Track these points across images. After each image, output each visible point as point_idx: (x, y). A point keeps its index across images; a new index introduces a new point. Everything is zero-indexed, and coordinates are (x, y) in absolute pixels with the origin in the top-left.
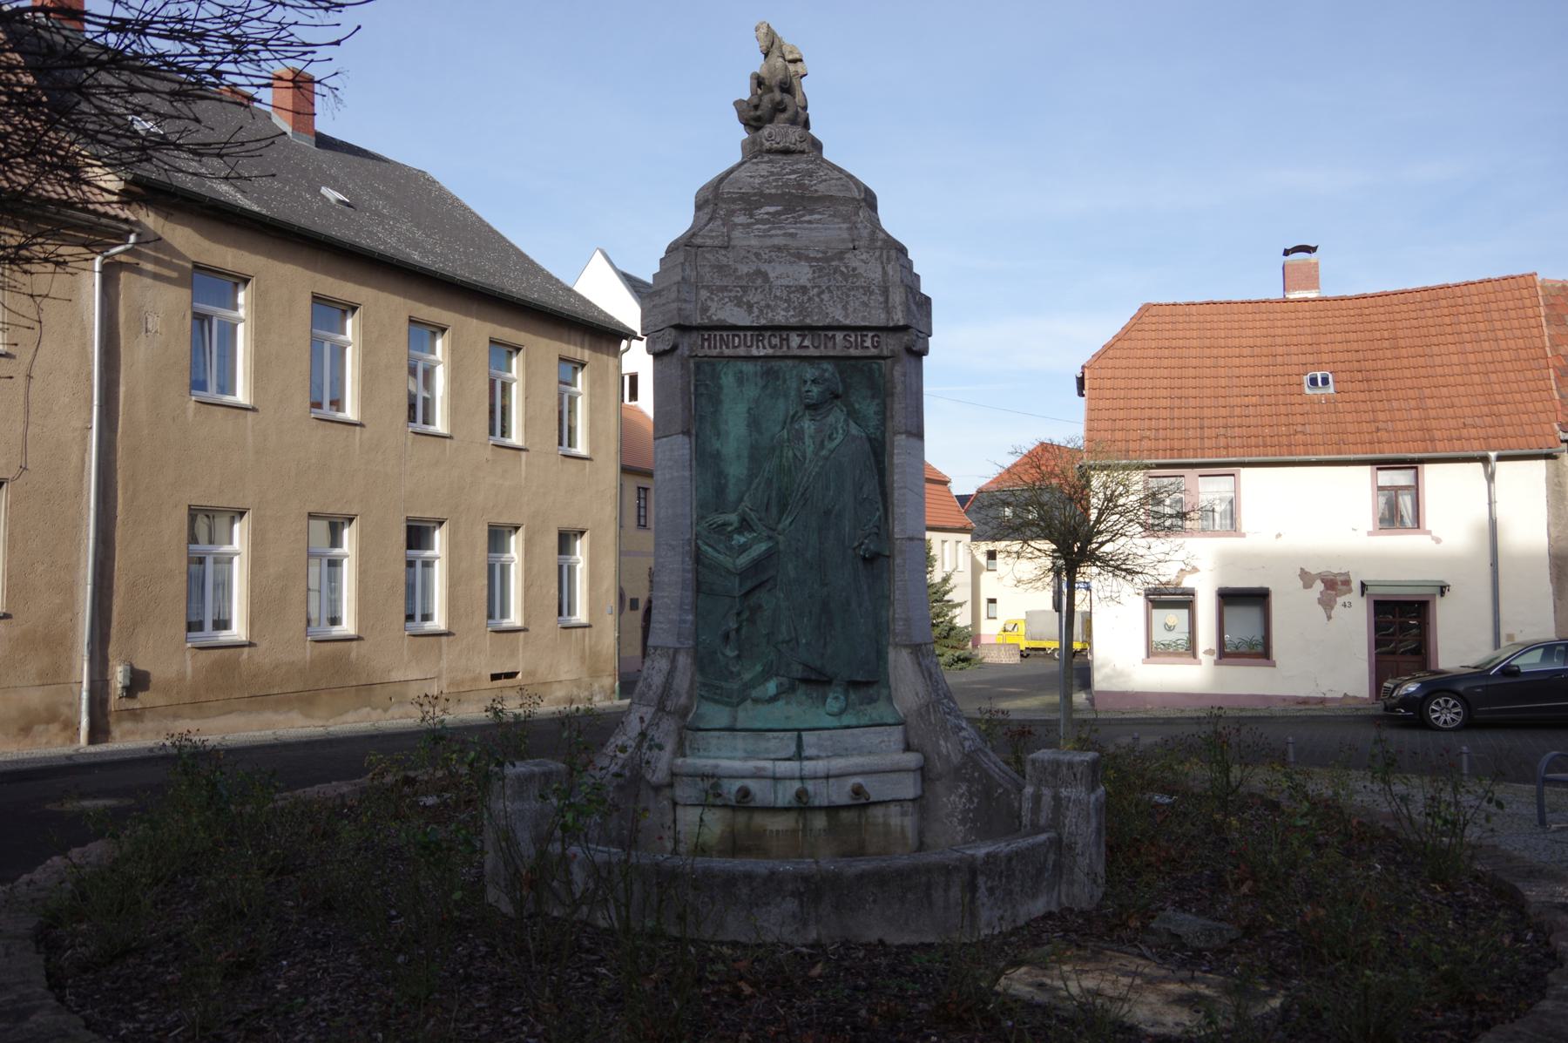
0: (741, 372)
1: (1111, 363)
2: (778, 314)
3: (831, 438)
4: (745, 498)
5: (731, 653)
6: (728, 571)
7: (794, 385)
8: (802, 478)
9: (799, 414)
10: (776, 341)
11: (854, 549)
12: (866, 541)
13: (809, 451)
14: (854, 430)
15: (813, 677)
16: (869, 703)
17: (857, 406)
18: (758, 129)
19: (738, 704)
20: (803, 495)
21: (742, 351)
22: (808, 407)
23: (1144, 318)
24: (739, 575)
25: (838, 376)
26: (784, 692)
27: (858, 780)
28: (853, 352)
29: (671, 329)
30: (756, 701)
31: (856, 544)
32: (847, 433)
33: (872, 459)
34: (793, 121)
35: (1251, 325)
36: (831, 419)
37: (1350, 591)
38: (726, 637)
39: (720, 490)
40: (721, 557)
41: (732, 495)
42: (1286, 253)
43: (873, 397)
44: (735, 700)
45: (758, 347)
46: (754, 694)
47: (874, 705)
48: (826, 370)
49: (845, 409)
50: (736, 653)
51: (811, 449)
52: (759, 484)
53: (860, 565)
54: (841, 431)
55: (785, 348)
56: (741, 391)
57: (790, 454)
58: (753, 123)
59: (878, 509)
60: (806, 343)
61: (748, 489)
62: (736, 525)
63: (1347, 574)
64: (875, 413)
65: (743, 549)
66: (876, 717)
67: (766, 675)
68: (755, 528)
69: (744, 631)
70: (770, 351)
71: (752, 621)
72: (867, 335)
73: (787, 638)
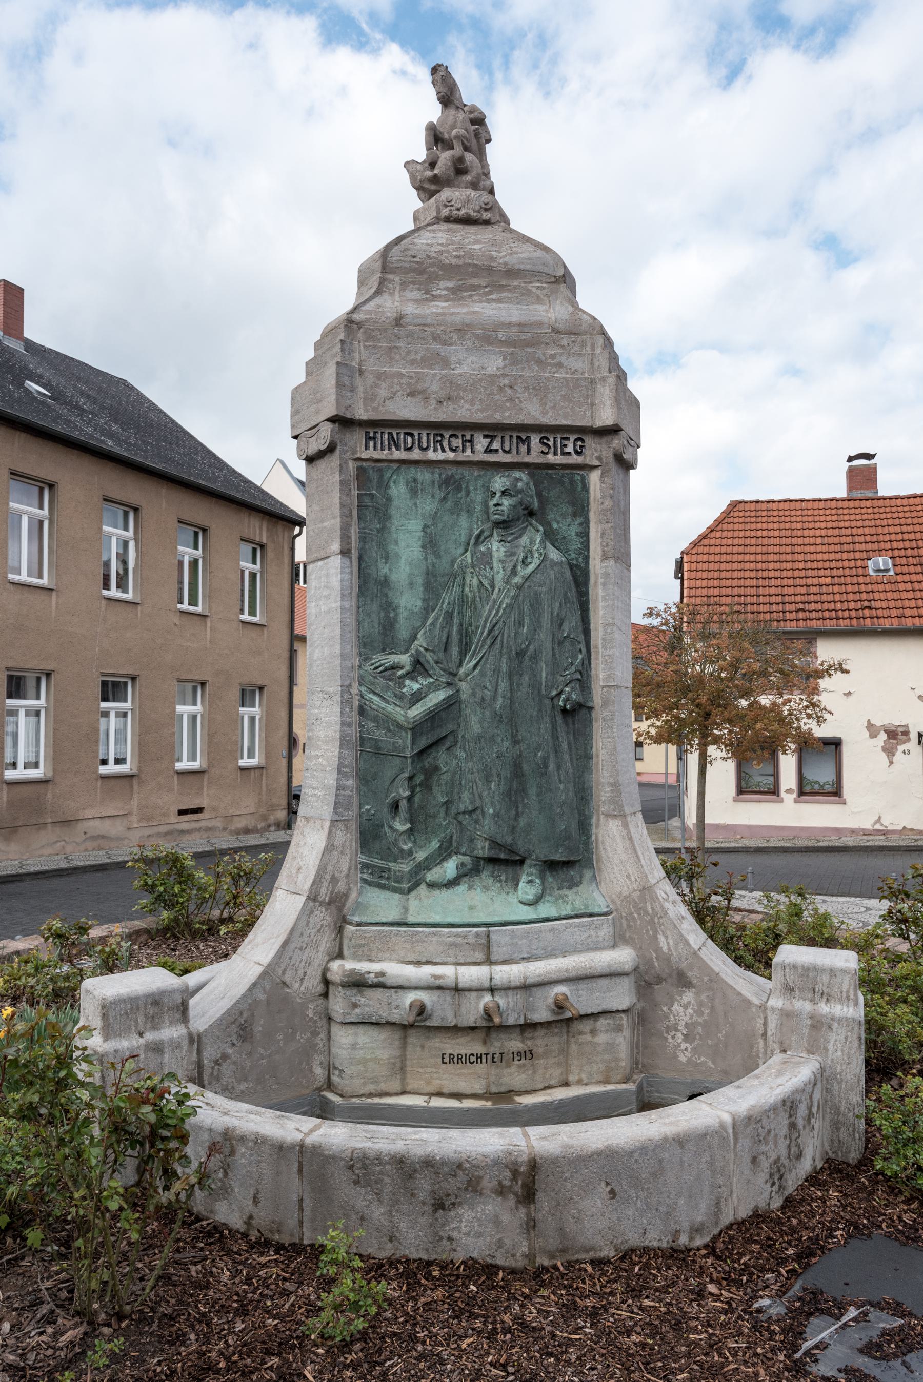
0: (415, 480)
1: (706, 550)
2: (461, 407)
3: (525, 563)
4: (419, 636)
5: (401, 826)
6: (400, 726)
7: (479, 499)
8: (490, 611)
9: (486, 534)
10: (456, 443)
11: (552, 699)
12: (567, 689)
13: (499, 578)
14: (554, 555)
15: (502, 856)
16: (570, 888)
17: (555, 526)
18: (432, 194)
19: (410, 890)
20: (490, 632)
21: (416, 455)
22: (498, 524)
23: (731, 514)
24: (412, 729)
25: (533, 487)
26: (466, 875)
27: (561, 989)
28: (551, 458)
29: (328, 423)
30: (432, 885)
31: (554, 693)
32: (545, 558)
33: (574, 589)
34: (474, 186)
35: (822, 518)
36: (525, 540)
37: (909, 740)
38: (395, 806)
39: (389, 626)
40: (390, 708)
41: (403, 631)
42: (850, 459)
43: (575, 515)
44: (405, 886)
45: (435, 450)
46: (430, 876)
47: (575, 890)
48: (519, 480)
49: (541, 528)
50: (408, 826)
51: (501, 575)
52: (436, 619)
53: (559, 719)
54: (536, 555)
55: (469, 452)
56: (415, 504)
57: (475, 582)
58: (427, 185)
59: (580, 650)
60: (496, 445)
61: (424, 624)
62: (408, 668)
63: (907, 726)
64: (577, 534)
65: (417, 698)
66: (580, 907)
67: (444, 853)
68: (431, 672)
69: (417, 799)
70: (451, 455)
71: (427, 786)
72: (568, 439)
73: (470, 808)
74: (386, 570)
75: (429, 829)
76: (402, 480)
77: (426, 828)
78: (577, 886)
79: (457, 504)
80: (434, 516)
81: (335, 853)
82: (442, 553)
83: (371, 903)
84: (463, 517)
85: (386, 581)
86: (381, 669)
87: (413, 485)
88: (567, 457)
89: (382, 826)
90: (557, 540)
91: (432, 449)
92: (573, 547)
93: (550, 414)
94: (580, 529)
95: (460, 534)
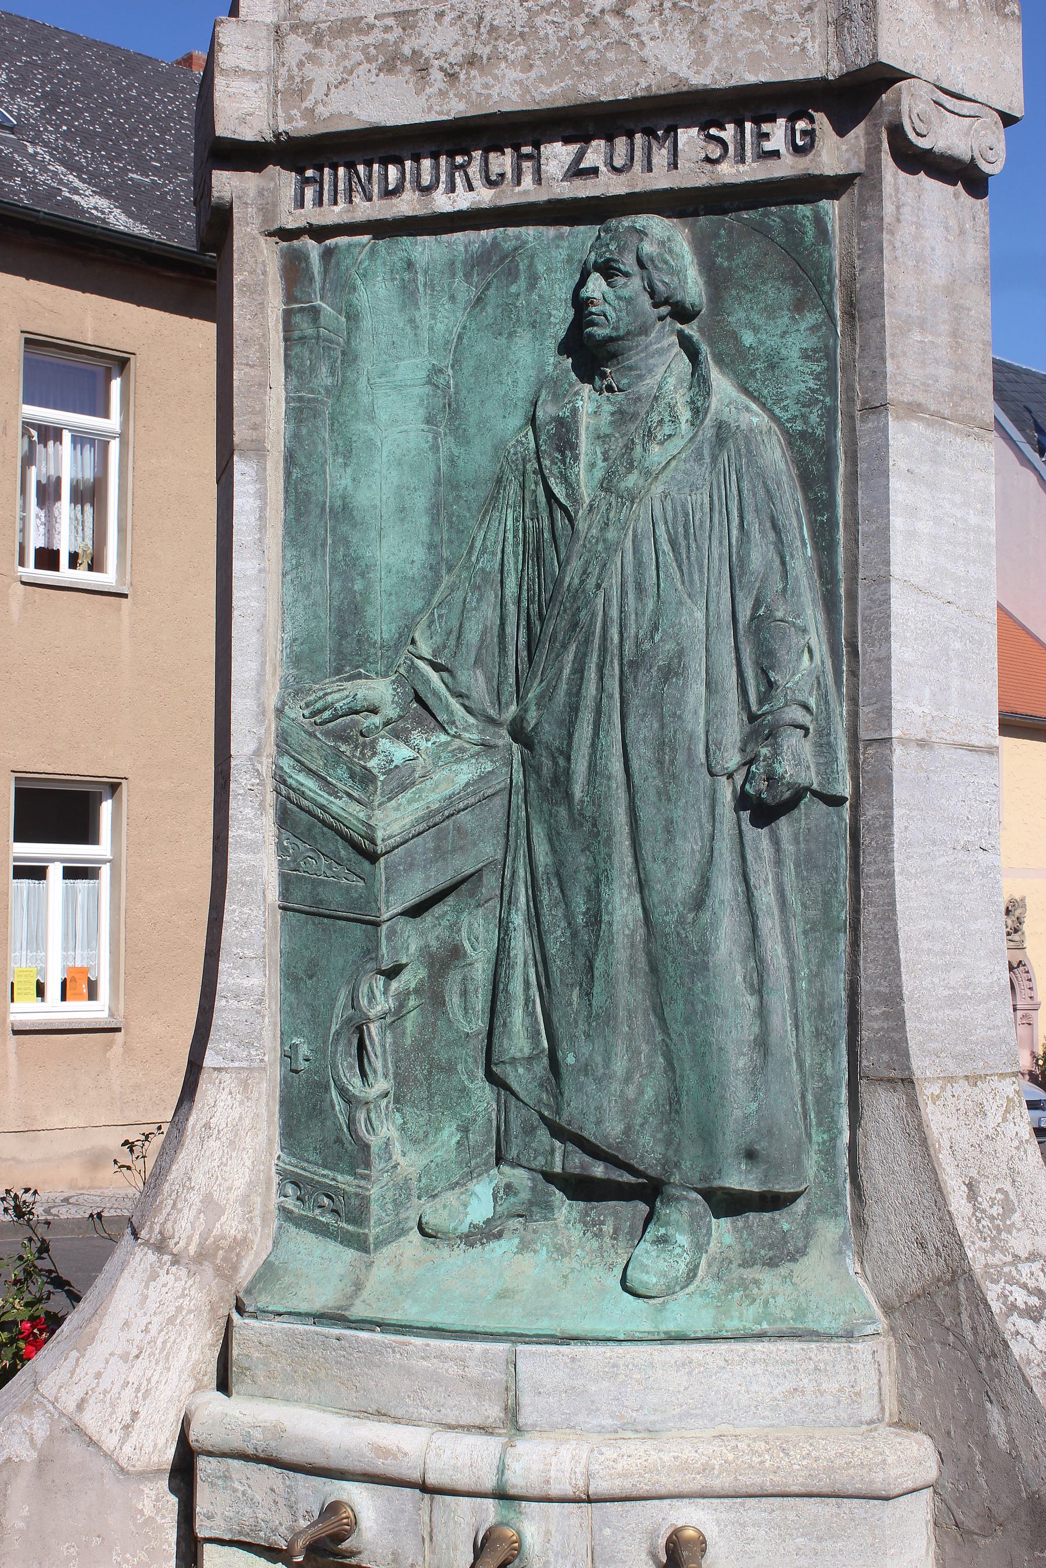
0: (410, 265)
17: (748, 339)
43: (799, 306)
55: (527, 180)
56: (412, 321)
64: (806, 356)
68: (442, 717)
74: (346, 481)
75: (437, 1099)
76: (380, 269)
77: (431, 1096)
78: (794, 1259)
79: (508, 308)
80: (458, 347)
81: (212, 1144)
82: (472, 431)
83: (291, 1266)
84: (524, 340)
85: (345, 506)
86: (326, 715)
87: (406, 276)
88: (771, 163)
89: (327, 1089)
90: (752, 374)
91: (442, 186)
92: (795, 389)
93: (715, 62)
94: (811, 342)
95: (515, 382)
